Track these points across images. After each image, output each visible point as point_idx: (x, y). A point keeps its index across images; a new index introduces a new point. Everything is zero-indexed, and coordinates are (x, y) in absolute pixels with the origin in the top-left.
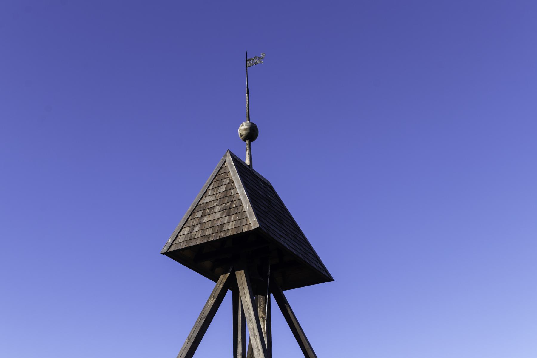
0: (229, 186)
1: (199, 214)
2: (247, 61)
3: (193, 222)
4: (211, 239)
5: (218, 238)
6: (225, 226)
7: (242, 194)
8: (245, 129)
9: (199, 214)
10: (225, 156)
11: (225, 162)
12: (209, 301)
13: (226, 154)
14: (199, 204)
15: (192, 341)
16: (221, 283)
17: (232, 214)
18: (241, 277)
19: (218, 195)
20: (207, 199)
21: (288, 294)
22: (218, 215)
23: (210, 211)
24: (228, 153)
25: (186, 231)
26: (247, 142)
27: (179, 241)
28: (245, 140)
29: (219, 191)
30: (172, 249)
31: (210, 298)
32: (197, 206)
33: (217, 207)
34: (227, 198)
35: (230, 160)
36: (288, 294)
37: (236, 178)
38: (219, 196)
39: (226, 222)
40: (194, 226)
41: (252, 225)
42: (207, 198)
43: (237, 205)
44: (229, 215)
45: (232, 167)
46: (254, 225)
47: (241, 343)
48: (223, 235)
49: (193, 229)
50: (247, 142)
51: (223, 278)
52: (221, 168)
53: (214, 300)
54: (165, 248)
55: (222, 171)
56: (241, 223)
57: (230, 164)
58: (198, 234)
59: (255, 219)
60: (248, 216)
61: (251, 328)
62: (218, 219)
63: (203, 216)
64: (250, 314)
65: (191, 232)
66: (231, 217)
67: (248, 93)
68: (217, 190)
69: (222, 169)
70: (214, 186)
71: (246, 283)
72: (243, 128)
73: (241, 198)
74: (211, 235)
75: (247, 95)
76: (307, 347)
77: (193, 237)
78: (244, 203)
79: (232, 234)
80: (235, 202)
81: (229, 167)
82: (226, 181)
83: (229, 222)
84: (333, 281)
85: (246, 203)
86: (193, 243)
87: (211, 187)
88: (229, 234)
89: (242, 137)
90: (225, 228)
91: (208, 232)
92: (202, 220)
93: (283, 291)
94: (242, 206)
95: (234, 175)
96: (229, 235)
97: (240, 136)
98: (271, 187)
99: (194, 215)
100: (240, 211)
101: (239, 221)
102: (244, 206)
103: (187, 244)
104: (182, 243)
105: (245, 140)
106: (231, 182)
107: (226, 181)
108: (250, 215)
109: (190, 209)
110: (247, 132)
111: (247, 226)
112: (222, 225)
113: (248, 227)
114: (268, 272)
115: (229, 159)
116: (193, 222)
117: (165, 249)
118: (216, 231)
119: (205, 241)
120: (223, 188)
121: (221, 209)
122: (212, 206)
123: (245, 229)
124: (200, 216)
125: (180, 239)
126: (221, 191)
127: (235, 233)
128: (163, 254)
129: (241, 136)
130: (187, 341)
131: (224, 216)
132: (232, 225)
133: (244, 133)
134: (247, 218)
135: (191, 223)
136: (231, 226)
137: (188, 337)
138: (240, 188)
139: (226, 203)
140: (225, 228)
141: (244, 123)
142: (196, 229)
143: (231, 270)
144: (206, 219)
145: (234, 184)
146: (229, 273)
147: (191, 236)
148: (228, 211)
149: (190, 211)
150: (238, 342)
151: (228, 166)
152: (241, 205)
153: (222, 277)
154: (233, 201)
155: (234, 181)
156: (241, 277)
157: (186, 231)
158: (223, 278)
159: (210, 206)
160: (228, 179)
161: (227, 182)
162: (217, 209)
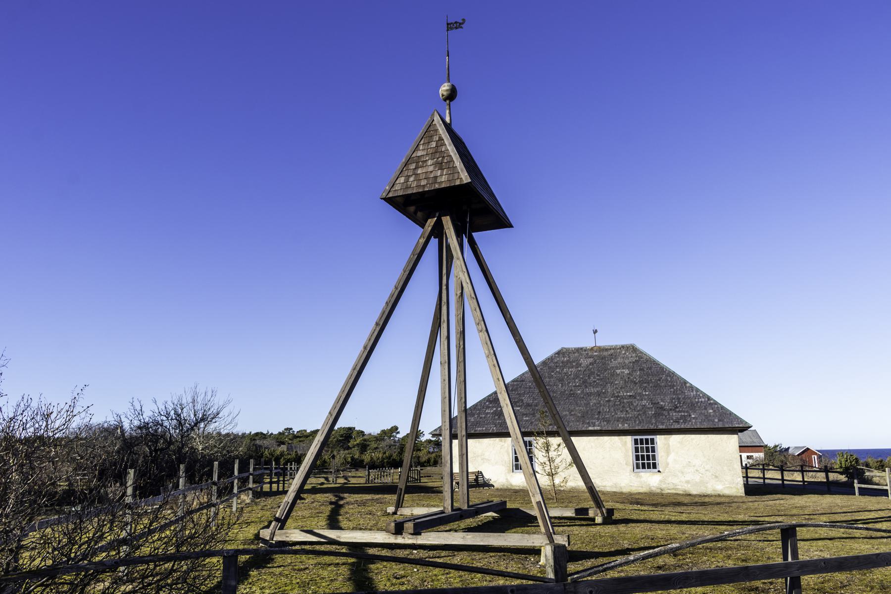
0: (440, 142)
1: (413, 166)
2: (448, 24)
3: (408, 173)
4: (426, 189)
5: (433, 189)
6: (438, 178)
7: (453, 151)
8: (447, 90)
9: (413, 166)
10: (433, 115)
11: (433, 120)
12: (420, 240)
13: (434, 113)
14: (412, 156)
15: (407, 273)
16: (429, 226)
17: (444, 168)
18: (447, 221)
19: (429, 150)
20: (419, 153)
21: (475, 235)
22: (431, 168)
23: (423, 164)
24: (436, 112)
25: (402, 180)
26: (448, 102)
27: (396, 189)
28: (445, 100)
29: (429, 147)
30: (390, 195)
31: (420, 238)
32: (410, 158)
33: (430, 161)
34: (438, 154)
35: (438, 119)
36: (475, 235)
37: (446, 136)
38: (430, 151)
39: (439, 175)
40: (409, 177)
41: (464, 180)
42: (419, 152)
43: (448, 160)
44: (441, 169)
45: (440, 125)
46: (466, 179)
47: (445, 276)
48: (437, 186)
49: (408, 179)
50: (448, 102)
51: (431, 222)
52: (430, 126)
53: (424, 240)
54: (384, 194)
55: (431, 128)
56: (453, 176)
57: (439, 122)
58: (414, 184)
59: (466, 174)
60: (460, 171)
61: (460, 265)
62: (431, 172)
63: (416, 168)
64: (457, 253)
65: (407, 181)
66: (444, 171)
67: (448, 56)
68: (428, 146)
69: (431, 127)
70: (424, 142)
71: (452, 227)
72: (445, 88)
73: (452, 154)
74: (426, 185)
75: (447, 57)
76: (491, 281)
77: (409, 186)
78: (454, 159)
79: (445, 186)
80: (446, 158)
81: (438, 125)
82: (436, 138)
83: (442, 175)
84: (511, 228)
85: (457, 159)
86: (409, 192)
87: (422, 142)
88: (443, 186)
89: (443, 97)
90: (439, 180)
91: (423, 183)
92: (416, 172)
93: (473, 233)
94: (452, 162)
95: (444, 133)
96: (443, 186)
97: (441, 96)
98: (464, 143)
99: (408, 167)
100: (451, 166)
101: (452, 175)
102: (455, 162)
103: (404, 192)
104: (399, 190)
105: (445, 100)
106: (441, 139)
107: (436, 138)
108: (462, 170)
109: (404, 160)
110: (448, 92)
111: (459, 180)
112: (436, 177)
113: (461, 181)
114: (467, 218)
115: (437, 118)
116: (408, 173)
117: (384, 195)
118: (431, 182)
119: (421, 190)
120: (434, 144)
121: (433, 163)
122: (425, 160)
123: (458, 183)
124: (414, 167)
125: (397, 187)
126: (432, 146)
127: (448, 185)
128: (381, 199)
129: (443, 95)
130: (403, 273)
131: (437, 169)
132: (445, 178)
133: (445, 93)
134: (459, 172)
135: (406, 173)
136: (444, 178)
137: (403, 270)
138: (450, 145)
139: (438, 158)
140: (439, 180)
141: (446, 84)
142: (412, 179)
143: (437, 215)
144: (419, 171)
145: (444, 142)
146: (436, 218)
147: (407, 185)
148: (440, 165)
149: (404, 163)
150: (443, 275)
151: (437, 125)
152: (452, 161)
153: (429, 220)
154: (444, 157)
155: (444, 138)
156: (447, 221)
157: (402, 180)
158: (431, 222)
159: (422, 160)
160: (438, 136)
161: (437, 139)
162: (430, 162)
